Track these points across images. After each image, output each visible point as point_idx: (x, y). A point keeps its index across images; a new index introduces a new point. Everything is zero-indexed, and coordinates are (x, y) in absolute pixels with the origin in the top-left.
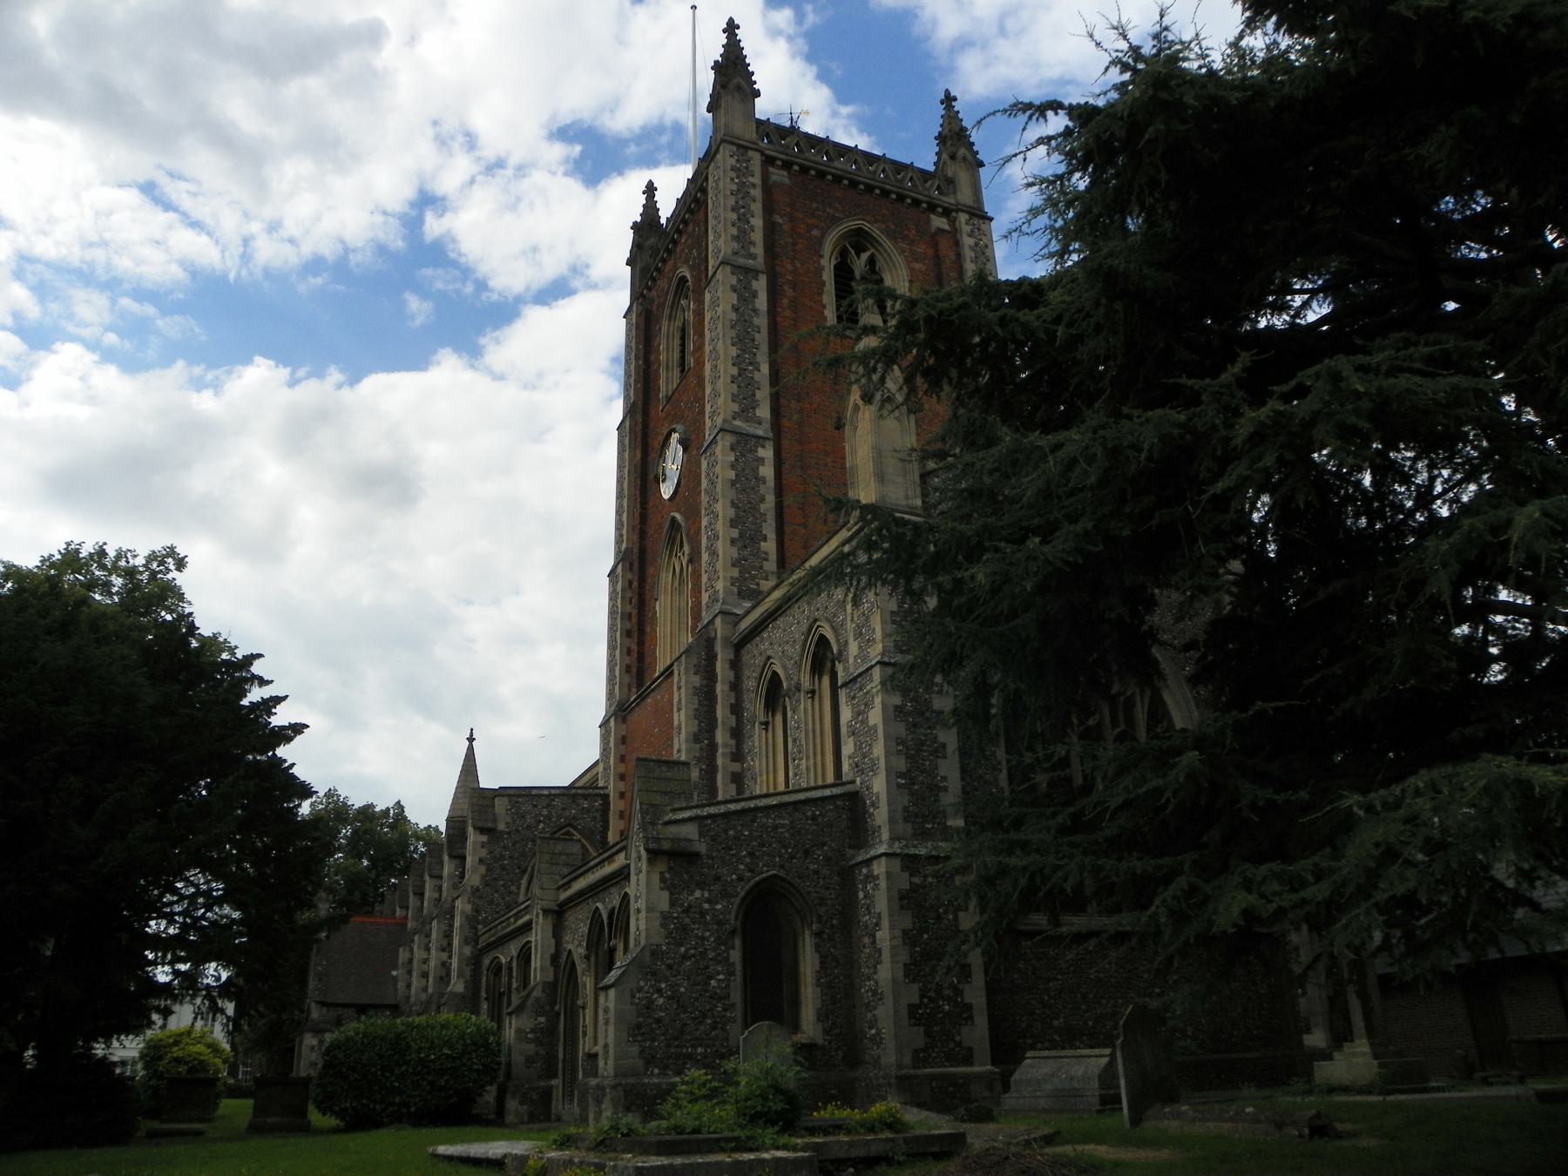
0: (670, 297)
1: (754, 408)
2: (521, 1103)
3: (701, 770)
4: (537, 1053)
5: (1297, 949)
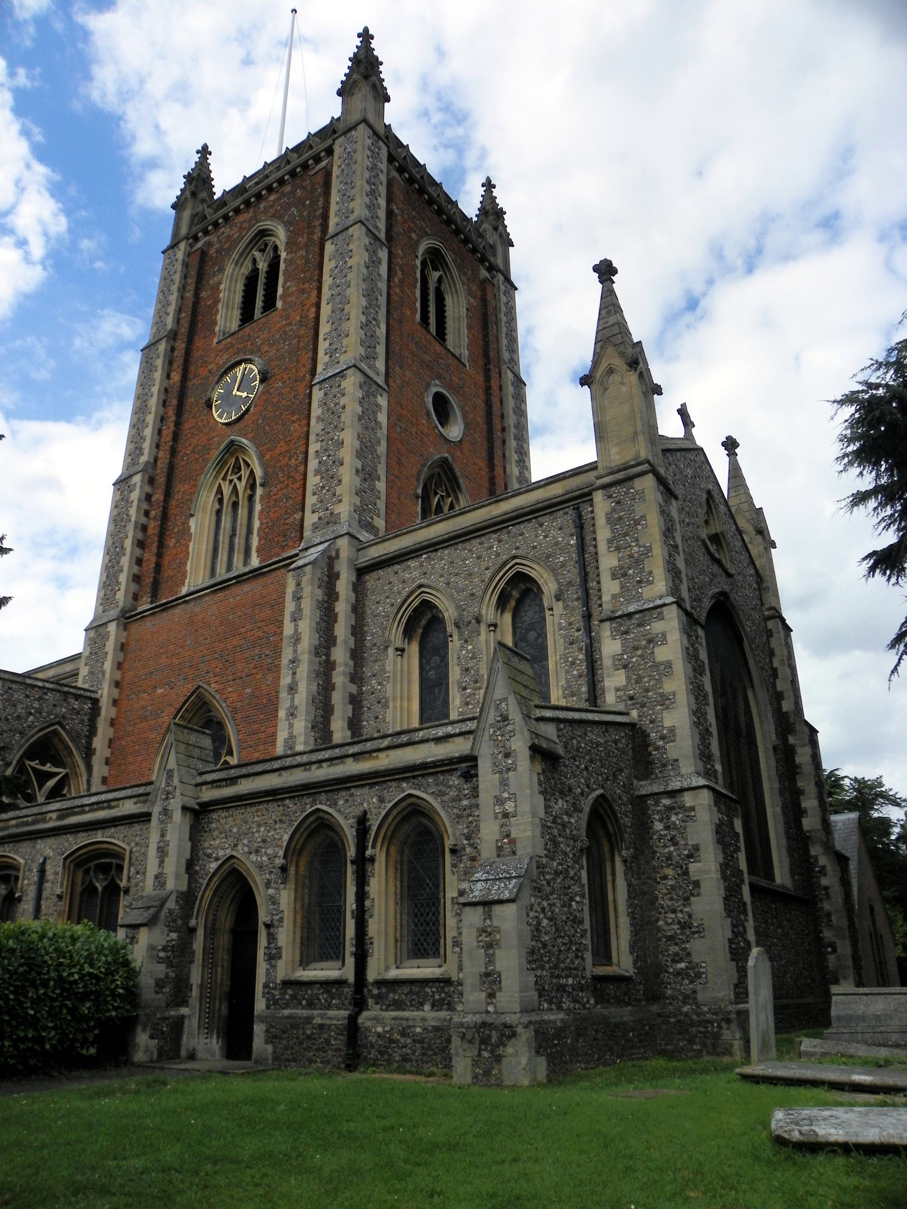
0: (242, 245)
1: (374, 359)
2: (152, 1037)
3: (319, 684)
4: (167, 976)
5: (829, 915)
